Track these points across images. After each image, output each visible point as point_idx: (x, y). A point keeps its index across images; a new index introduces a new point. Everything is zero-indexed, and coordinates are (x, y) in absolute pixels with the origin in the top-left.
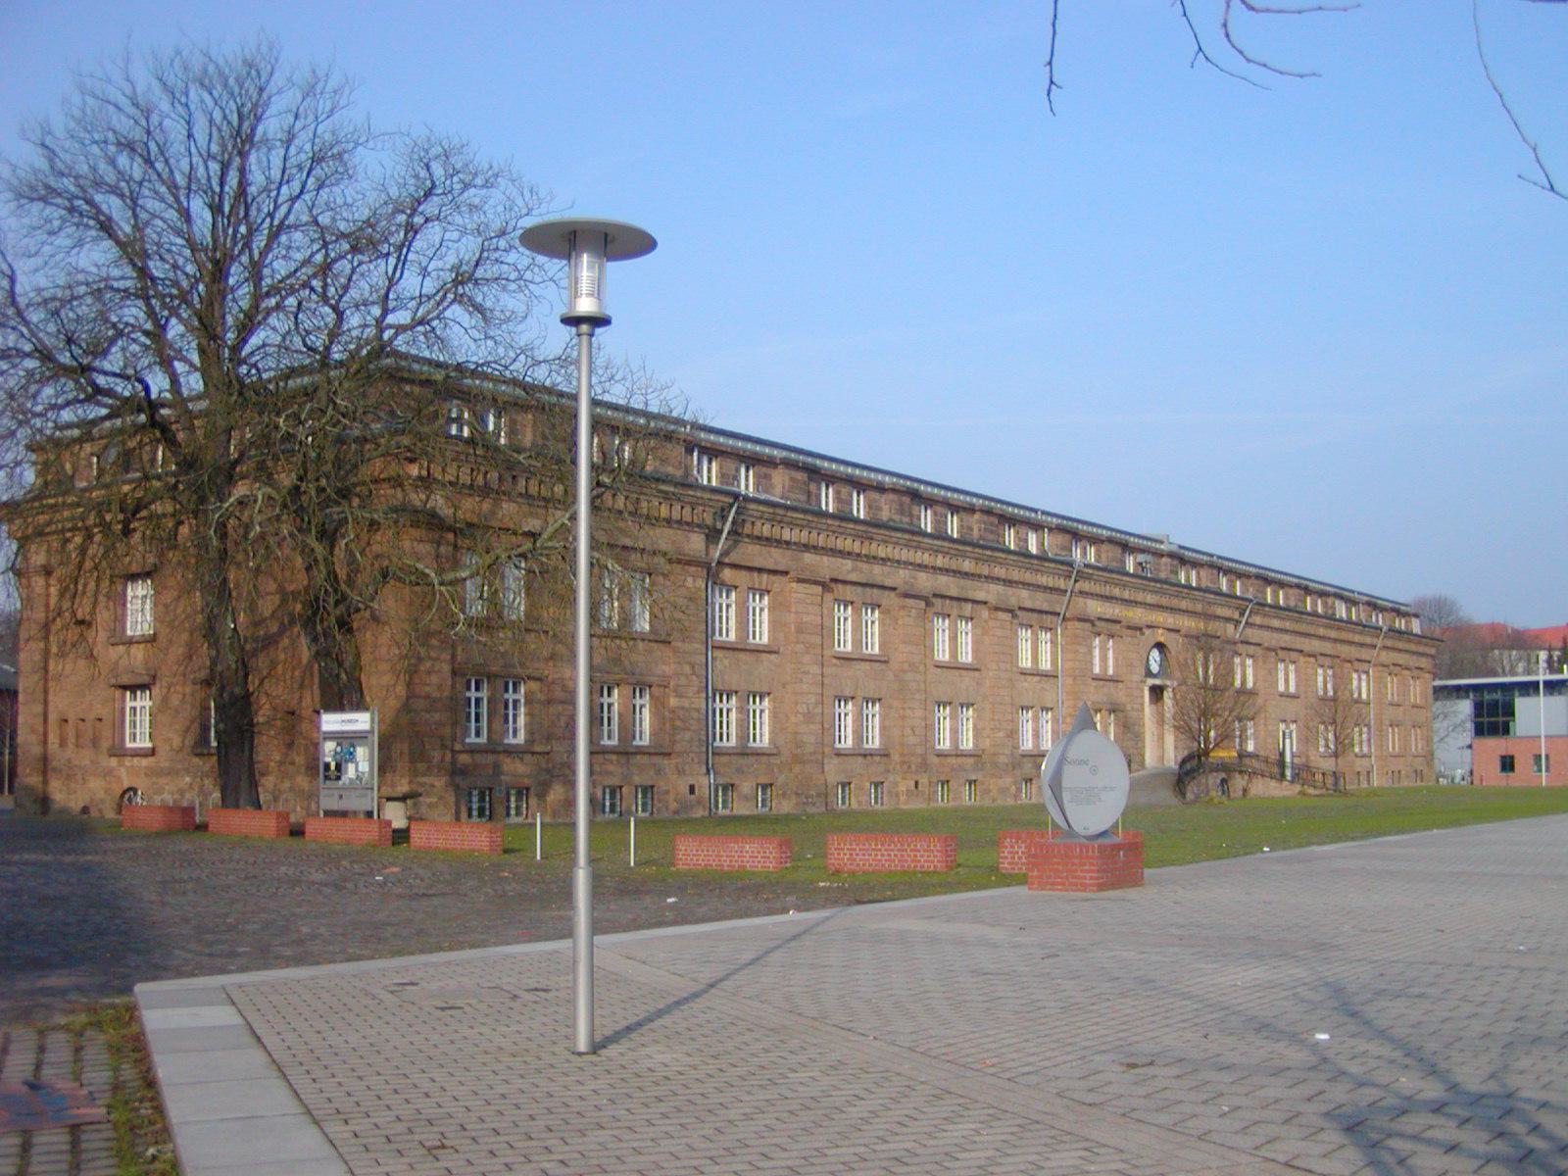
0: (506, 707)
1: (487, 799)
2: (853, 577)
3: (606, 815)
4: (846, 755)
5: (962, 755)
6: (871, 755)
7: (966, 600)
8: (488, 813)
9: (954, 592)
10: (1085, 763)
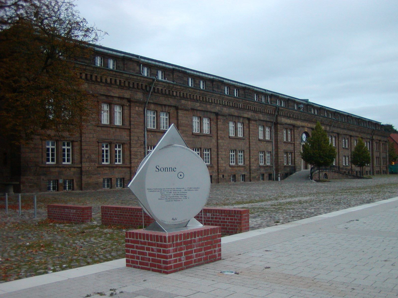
0: (116, 153)
1: (72, 183)
2: (199, 108)
5: (240, 167)
7: (241, 117)
8: (110, 186)
9: (236, 114)
10: (173, 170)
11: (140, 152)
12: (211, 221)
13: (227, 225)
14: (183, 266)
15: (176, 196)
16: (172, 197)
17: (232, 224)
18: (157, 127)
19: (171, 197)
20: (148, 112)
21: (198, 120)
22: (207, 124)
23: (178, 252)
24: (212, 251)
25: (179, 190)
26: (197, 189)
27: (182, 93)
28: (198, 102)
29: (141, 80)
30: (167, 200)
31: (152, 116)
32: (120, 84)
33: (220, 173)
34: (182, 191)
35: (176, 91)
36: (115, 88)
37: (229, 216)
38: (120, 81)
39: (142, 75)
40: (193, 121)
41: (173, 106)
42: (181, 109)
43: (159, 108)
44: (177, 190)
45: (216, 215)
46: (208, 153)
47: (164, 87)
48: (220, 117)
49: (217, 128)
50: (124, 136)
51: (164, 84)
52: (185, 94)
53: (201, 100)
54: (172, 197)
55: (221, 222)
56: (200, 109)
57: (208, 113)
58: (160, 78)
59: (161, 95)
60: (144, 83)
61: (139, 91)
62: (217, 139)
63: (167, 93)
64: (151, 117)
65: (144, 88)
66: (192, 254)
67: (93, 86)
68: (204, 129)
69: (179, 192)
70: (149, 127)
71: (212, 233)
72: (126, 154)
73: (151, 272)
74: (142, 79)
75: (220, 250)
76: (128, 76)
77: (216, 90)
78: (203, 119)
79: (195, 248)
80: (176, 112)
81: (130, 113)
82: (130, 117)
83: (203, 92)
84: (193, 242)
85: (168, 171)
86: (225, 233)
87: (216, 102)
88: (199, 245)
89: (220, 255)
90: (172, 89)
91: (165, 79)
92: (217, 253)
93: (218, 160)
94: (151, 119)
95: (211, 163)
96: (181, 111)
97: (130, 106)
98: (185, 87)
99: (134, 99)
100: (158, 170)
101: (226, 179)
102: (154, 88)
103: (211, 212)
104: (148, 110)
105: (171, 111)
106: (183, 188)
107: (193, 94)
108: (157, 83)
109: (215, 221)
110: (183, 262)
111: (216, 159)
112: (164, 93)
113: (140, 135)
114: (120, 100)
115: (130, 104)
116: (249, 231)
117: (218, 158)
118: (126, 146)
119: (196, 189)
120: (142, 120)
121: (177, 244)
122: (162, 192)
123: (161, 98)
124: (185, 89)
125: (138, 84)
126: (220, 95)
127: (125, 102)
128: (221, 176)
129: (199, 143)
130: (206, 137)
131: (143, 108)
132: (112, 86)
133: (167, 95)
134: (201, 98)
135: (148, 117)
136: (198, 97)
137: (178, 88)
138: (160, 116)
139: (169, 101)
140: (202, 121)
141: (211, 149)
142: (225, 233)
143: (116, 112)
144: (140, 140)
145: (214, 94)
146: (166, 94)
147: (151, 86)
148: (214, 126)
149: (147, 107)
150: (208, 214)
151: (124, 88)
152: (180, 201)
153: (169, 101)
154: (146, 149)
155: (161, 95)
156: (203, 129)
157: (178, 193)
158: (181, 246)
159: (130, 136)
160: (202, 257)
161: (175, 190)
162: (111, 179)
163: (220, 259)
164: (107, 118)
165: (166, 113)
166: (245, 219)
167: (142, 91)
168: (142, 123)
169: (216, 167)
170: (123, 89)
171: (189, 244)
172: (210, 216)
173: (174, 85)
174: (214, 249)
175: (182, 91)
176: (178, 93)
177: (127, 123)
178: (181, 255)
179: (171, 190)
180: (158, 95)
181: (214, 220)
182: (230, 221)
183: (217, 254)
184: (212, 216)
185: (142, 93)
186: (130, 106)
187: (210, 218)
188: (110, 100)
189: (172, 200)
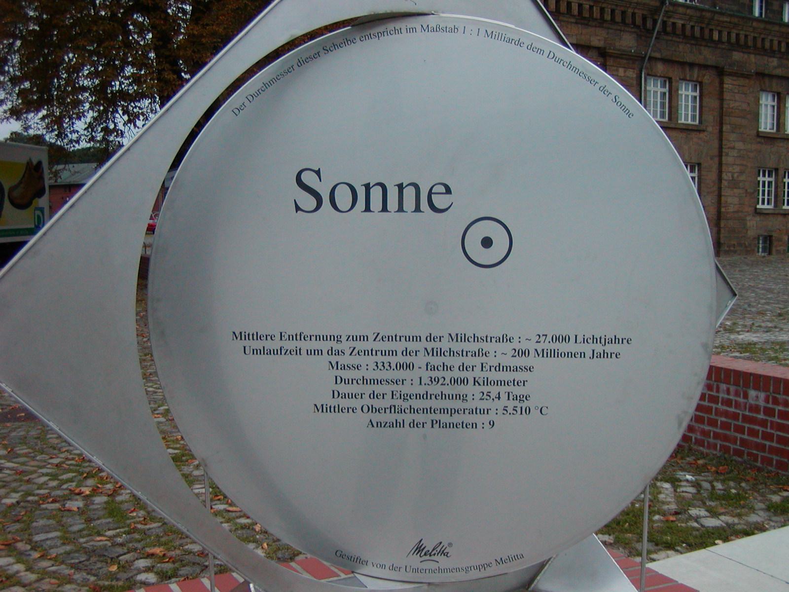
2: (778, 72)
3: (760, 254)
12: (763, 423)
15: (447, 390)
16: (418, 396)
18: (670, 118)
19: (405, 397)
20: (648, 81)
21: (774, 101)
25: (473, 347)
26: (609, 348)
27: (734, 35)
28: (774, 57)
30: (376, 417)
31: (660, 90)
34: (492, 361)
35: (719, 28)
36: (568, 22)
40: (761, 102)
41: (712, 67)
42: (731, 74)
43: (675, 73)
44: (457, 347)
46: (770, 179)
52: (742, 38)
54: (418, 396)
56: (780, 74)
59: (681, 40)
60: (639, 9)
63: (697, 33)
65: (639, 21)
69: (469, 361)
78: (785, 98)
80: (717, 83)
85: (385, 209)
90: (708, 24)
94: (655, 97)
96: (731, 77)
98: (743, 18)
99: (614, 50)
100: (312, 202)
102: (664, 23)
103: (766, 390)
104: (648, 77)
105: (706, 77)
106: (505, 339)
107: (762, 36)
108: (671, 8)
112: (690, 35)
119: (599, 348)
122: (344, 360)
125: (623, 13)
129: (772, 157)
135: (648, 93)
136: (776, 43)
137: (723, 22)
139: (700, 53)
140: (782, 105)
146: (693, 37)
147: (656, 17)
149: (647, 68)
151: (590, 23)
152: (474, 425)
153: (700, 53)
155: (681, 40)
157: (463, 368)
161: (436, 345)
165: (694, 83)
167: (633, 30)
170: (587, 25)
172: (762, 403)
176: (725, 34)
179: (412, 346)
180: (674, 39)
181: (776, 419)
184: (770, 406)
187: (758, 412)
189: (420, 418)
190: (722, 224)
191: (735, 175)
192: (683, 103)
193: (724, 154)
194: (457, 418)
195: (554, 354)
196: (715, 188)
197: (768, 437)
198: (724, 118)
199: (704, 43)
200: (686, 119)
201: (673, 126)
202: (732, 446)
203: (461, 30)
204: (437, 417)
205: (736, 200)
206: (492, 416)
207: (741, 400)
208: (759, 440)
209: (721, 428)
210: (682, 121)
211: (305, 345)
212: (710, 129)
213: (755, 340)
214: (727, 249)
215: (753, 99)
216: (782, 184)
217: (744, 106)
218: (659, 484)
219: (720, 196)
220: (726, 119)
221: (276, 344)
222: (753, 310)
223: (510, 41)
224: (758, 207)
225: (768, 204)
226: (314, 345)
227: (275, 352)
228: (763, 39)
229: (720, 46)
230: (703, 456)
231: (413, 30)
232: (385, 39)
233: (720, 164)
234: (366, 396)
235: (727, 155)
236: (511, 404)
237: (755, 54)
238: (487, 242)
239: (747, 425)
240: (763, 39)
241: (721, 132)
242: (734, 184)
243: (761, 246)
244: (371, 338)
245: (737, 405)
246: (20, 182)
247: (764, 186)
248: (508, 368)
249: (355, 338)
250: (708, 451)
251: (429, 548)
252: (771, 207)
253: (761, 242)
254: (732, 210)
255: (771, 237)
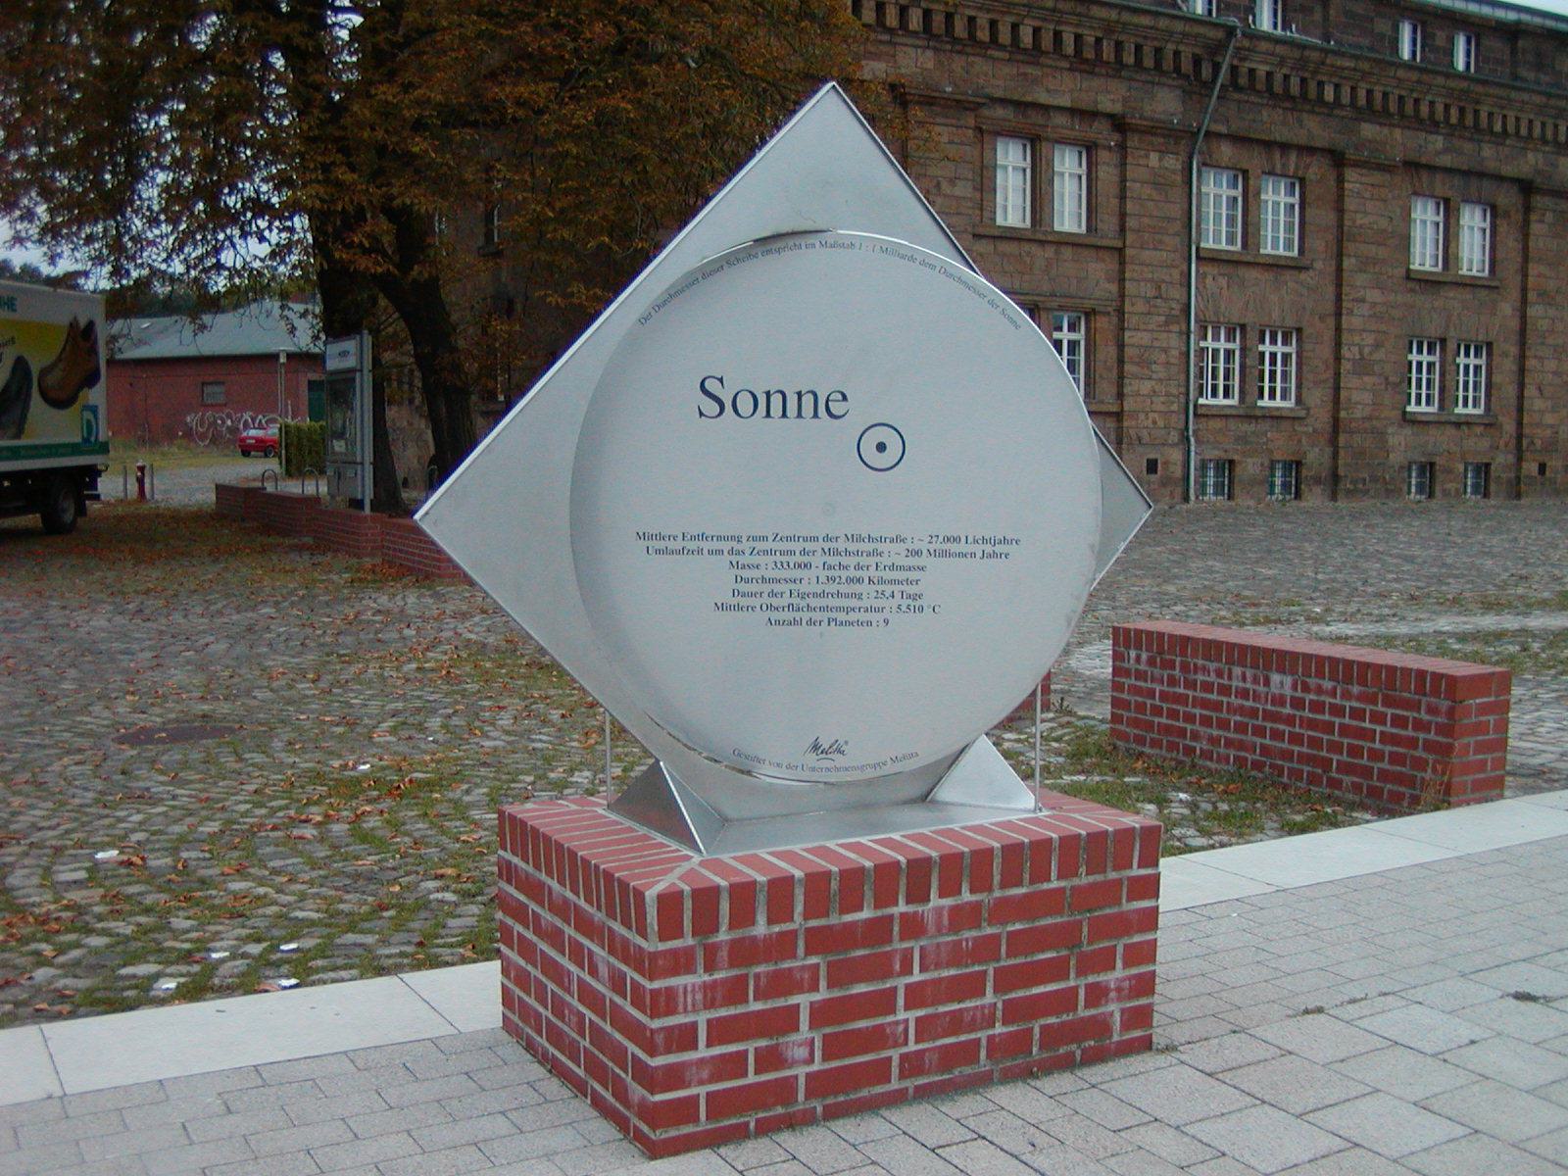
2: (1446, 160)
3: (1412, 496)
4: (1427, 423)
6: (1468, 424)
10: (827, 407)
11: (1165, 350)
12: (1290, 720)
13: (1376, 755)
14: (801, 1096)
15: (844, 589)
16: (816, 595)
17: (1401, 750)
19: (802, 596)
20: (1204, 175)
22: (1478, 235)
23: (756, 1006)
24: (1075, 990)
25: (869, 547)
26: (999, 549)
28: (1437, 133)
29: (1171, 34)
30: (775, 616)
31: (1226, 192)
32: (1076, 52)
33: (1527, 455)
34: (885, 561)
35: (1335, 80)
37: (1389, 702)
38: (1078, 38)
39: (1180, 8)
41: (1323, 150)
42: (1356, 164)
43: (1254, 160)
44: (852, 547)
45: (1320, 690)
46: (1431, 358)
47: (1282, 62)
48: (1538, 201)
49: (1525, 249)
50: (1096, 278)
51: (1279, 49)
52: (1378, 96)
53: (1454, 120)
54: (816, 595)
55: (1345, 730)
57: (1486, 183)
58: (1265, 22)
60: (1187, 44)
61: (1164, 80)
62: (1524, 301)
64: (1217, 197)
65: (1187, 66)
66: (890, 1019)
67: (958, 63)
68: (1465, 253)
69: (864, 560)
70: (1209, 244)
71: (1083, 870)
72: (1101, 355)
73: (582, 1108)
74: (1179, 26)
75: (1145, 985)
76: (1113, 15)
77: (1531, 75)
79: (917, 976)
80: (1332, 177)
81: (1123, 180)
82: (1123, 197)
83: (1464, 85)
84: (896, 929)
86: (1357, 798)
87: (1524, 131)
88: (957, 956)
89: (1141, 1017)
90: (1315, 72)
91: (1286, 26)
92: (1114, 1009)
93: (1521, 397)
95: (1488, 408)
97: (1122, 147)
101: (1553, 482)
102: (1234, 69)
104: (1204, 169)
107: (1415, 95)
108: (1246, 43)
109: (1312, 724)
110: (801, 1071)
111: (1511, 391)
113: (1167, 278)
114: (1077, 121)
115: (1124, 140)
116: (1501, 797)
117: (1521, 386)
118: (1102, 323)
119: (989, 548)
120: (1176, 210)
121: (745, 952)
122: (743, 560)
123: (1265, 113)
124: (1375, 71)
125: (1158, 51)
126: (1544, 100)
127: (1101, 131)
128: (1531, 468)
129: (1435, 316)
130: (1468, 289)
131: (1183, 156)
132: (1042, 60)
133: (1293, 98)
134: (1454, 112)
135: (1204, 201)
136: (1440, 108)
137: (1343, 69)
138: (1258, 193)
139: (1301, 127)
140: (1452, 221)
141: (1489, 345)
142: (1357, 798)
143: (1062, 174)
144: (1166, 300)
145: (1513, 95)
146: (1287, 96)
147: (1219, 59)
148: (1511, 243)
150: (1275, 678)
154: (1192, 336)
156: (1457, 258)
157: (858, 567)
158: (786, 965)
159: (1122, 280)
160: (982, 1035)
161: (833, 545)
162: (1231, 462)
163: (1146, 1045)
164: (1075, 209)
165: (1289, 180)
166: (1481, 729)
168: (1177, 226)
169: (1509, 427)
170: (1092, 73)
171: (856, 946)
172: (1288, 692)
173: (1326, 51)
174: (1091, 979)
175: (1362, 79)
176: (1346, 91)
177: (1108, 224)
178: (787, 1020)
179: (809, 546)
180: (1252, 98)
181: (1307, 714)
182: (1388, 729)
183: (1117, 1016)
184: (1299, 694)
185: (1178, 92)
186: (1122, 147)
187: (1282, 704)
188: (1034, 125)
189: (817, 616)
190: (1342, 439)
191: (1367, 350)
192: (1270, 217)
193: (1344, 311)
194: (853, 616)
195: (945, 554)
196: (1330, 374)
197: (1295, 739)
198: (1345, 244)
199: (1308, 107)
200: (1275, 246)
201: (1249, 258)
202: (1250, 757)
203: (857, 245)
204: (833, 615)
205: (1367, 397)
206: (886, 614)
207: (1261, 689)
208: (1285, 745)
209: (1236, 730)
210: (1267, 249)
211: (706, 546)
212: (1318, 265)
213: (1350, 633)
214: (1352, 487)
215: (1398, 211)
216: (1454, 368)
217: (1383, 223)
218: (1139, 805)
219: (1337, 389)
220: (1350, 247)
221: (678, 545)
222: (1370, 590)
223: (903, 257)
224: (1409, 409)
225: (1428, 403)
226: (716, 545)
227: (678, 552)
228: (1417, 101)
229: (1337, 112)
230: (1210, 773)
231: (813, 246)
232: (788, 253)
233: (1338, 329)
234: (765, 595)
235: (1351, 312)
236: (905, 603)
237: (1403, 128)
238: (881, 447)
239: (1269, 725)
240: (1417, 101)
241: (1339, 269)
242: (1363, 367)
243: (1414, 482)
244: (771, 539)
245: (1256, 697)
246: (59, 359)
247: (1467, 373)
248: (901, 568)
249: (754, 539)
250: (1219, 767)
251: (826, 746)
252: (1434, 409)
253: (1414, 474)
254: (1359, 415)
255: (1432, 465)
